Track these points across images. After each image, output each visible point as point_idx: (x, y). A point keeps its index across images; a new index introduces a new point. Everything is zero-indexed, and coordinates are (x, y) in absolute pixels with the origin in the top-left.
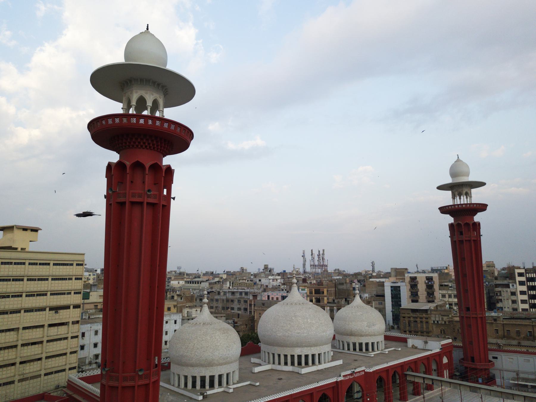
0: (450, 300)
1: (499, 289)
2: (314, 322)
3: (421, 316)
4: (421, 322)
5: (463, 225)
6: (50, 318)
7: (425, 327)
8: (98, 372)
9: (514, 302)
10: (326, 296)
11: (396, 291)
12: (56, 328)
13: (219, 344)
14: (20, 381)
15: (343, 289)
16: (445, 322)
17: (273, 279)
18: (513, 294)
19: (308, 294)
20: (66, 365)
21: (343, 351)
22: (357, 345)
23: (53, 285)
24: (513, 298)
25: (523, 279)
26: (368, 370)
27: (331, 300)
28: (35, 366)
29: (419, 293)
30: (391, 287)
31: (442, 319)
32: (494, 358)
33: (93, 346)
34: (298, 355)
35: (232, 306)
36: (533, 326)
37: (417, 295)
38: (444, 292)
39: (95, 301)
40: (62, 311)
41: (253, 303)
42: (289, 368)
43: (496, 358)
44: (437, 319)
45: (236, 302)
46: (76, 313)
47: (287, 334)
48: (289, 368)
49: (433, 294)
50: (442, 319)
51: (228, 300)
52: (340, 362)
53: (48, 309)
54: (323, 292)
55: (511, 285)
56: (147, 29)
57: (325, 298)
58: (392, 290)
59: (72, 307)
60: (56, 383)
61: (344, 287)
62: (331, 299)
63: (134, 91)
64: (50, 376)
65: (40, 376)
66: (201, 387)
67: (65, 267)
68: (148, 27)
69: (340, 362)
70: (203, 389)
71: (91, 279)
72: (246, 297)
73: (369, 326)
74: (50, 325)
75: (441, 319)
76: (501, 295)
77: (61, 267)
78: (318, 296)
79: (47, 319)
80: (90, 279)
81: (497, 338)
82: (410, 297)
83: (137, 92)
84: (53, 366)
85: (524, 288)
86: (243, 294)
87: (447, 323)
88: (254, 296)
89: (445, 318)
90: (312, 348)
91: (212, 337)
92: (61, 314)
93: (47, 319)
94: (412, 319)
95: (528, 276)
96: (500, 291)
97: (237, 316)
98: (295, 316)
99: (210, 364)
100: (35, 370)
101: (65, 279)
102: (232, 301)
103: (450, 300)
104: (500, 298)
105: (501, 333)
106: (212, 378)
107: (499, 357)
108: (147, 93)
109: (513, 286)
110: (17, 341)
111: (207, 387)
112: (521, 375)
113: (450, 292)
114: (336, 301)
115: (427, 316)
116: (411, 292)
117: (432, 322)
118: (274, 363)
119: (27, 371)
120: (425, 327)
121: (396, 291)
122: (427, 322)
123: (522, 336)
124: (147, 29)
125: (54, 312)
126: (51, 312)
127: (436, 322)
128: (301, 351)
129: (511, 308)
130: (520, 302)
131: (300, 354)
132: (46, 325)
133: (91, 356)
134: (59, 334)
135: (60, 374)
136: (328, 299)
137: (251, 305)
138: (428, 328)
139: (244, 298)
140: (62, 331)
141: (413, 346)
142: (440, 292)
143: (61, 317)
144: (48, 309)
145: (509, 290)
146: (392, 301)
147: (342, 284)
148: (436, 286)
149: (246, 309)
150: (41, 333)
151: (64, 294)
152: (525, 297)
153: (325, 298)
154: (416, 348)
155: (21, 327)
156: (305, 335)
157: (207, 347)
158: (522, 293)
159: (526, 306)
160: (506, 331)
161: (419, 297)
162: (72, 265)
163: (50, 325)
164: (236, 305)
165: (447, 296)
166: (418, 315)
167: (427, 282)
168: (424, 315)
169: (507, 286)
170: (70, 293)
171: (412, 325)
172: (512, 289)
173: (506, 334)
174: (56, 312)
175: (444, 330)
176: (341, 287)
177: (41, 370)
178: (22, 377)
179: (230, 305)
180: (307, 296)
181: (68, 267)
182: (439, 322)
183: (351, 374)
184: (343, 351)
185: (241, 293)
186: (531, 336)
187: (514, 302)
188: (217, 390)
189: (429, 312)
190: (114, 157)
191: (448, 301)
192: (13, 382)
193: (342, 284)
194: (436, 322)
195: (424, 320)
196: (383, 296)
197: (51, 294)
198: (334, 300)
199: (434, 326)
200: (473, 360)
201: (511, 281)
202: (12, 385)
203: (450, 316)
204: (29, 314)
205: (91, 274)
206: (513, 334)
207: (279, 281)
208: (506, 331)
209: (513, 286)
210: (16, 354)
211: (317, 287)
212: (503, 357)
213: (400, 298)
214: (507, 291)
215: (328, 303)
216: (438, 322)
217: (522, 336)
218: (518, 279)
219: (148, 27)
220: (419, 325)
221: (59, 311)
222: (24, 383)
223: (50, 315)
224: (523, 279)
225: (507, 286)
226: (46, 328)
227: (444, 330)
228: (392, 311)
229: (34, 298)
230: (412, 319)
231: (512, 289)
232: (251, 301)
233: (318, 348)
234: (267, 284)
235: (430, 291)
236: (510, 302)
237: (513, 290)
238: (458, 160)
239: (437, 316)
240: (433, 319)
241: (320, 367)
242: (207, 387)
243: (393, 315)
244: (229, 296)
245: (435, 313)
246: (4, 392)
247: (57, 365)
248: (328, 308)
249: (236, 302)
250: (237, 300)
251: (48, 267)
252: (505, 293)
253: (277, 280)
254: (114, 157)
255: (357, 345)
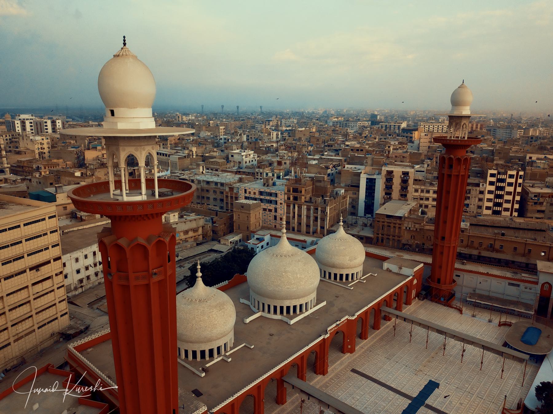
0: (422, 194)
1: (469, 188)
2: (303, 276)
3: (395, 222)
6: (32, 278)
7: (397, 231)
9: (480, 200)
10: (304, 196)
11: (371, 184)
12: (40, 284)
14: (15, 341)
18: (482, 192)
19: (286, 191)
20: (57, 313)
23: (28, 246)
24: (481, 196)
25: (493, 179)
26: (351, 318)
27: (308, 199)
28: (27, 324)
29: (393, 186)
30: (367, 179)
31: (414, 226)
32: (457, 276)
33: (76, 272)
35: (208, 196)
37: (391, 188)
38: (417, 187)
39: (63, 202)
40: (43, 268)
41: (229, 195)
42: (278, 317)
43: (459, 276)
44: (410, 226)
45: (211, 192)
46: (58, 264)
47: (277, 289)
48: (278, 317)
49: (406, 188)
50: (414, 226)
51: (202, 190)
53: (28, 270)
54: (301, 192)
55: (481, 184)
56: (125, 44)
58: (367, 182)
59: (52, 261)
60: (51, 331)
61: (322, 184)
62: (308, 197)
63: (121, 148)
64: (43, 328)
65: (34, 330)
66: (201, 358)
67: (37, 224)
68: (124, 41)
69: (324, 303)
70: (202, 360)
71: (45, 144)
72: (222, 188)
73: (350, 260)
74: (34, 284)
76: (470, 193)
77: (33, 225)
79: (29, 279)
80: (43, 144)
81: (462, 247)
82: (384, 189)
84: (45, 318)
85: (493, 188)
86: (219, 185)
87: (418, 230)
89: (417, 226)
90: (300, 299)
91: (209, 317)
92: (42, 270)
93: (29, 279)
94: (386, 224)
98: (286, 272)
99: (210, 340)
100: (27, 327)
101: (40, 236)
102: (207, 191)
103: (422, 194)
104: (469, 195)
105: (465, 243)
106: (211, 351)
107: (461, 276)
108: (137, 150)
109: (483, 185)
110: (4, 308)
111: (207, 358)
113: (423, 187)
115: (400, 222)
118: (263, 311)
119: (21, 330)
120: (397, 231)
122: (400, 228)
123: (483, 247)
124: (125, 44)
125: (35, 270)
126: (32, 272)
127: (408, 228)
128: (290, 303)
130: (485, 208)
132: (30, 285)
133: (76, 281)
134: (44, 288)
135: (53, 323)
137: (227, 197)
138: (399, 232)
139: (219, 189)
140: (47, 284)
141: (388, 269)
142: (414, 186)
143: (43, 273)
144: (28, 270)
145: (478, 189)
146: (366, 192)
147: (320, 181)
148: (411, 181)
149: (222, 200)
150: (26, 293)
151: (42, 251)
153: (303, 197)
154: (390, 271)
155: (5, 295)
156: (295, 289)
157: (206, 327)
158: (490, 192)
160: (470, 242)
162: (44, 219)
163: (34, 284)
164: (211, 195)
165: (420, 191)
166: (392, 220)
167: (402, 176)
168: (398, 221)
170: (47, 248)
171: (385, 229)
172: (481, 188)
173: (469, 244)
174: (38, 270)
175: (414, 237)
176: (318, 184)
177: (33, 326)
178: (16, 337)
179: (206, 195)
180: (285, 194)
181: (40, 223)
182: (411, 229)
183: (336, 327)
186: (491, 247)
189: (403, 219)
192: (9, 344)
193: (320, 181)
194: (408, 228)
195: (397, 225)
196: (358, 187)
197: (28, 255)
198: (311, 198)
199: (406, 232)
200: (439, 281)
201: (482, 181)
202: (9, 347)
203: (422, 224)
204: (9, 280)
205: (44, 138)
206: (476, 244)
207: (252, 156)
208: (470, 242)
210: (6, 320)
212: (465, 276)
213: (374, 190)
214: (476, 190)
215: (305, 202)
216: (410, 228)
217: (483, 247)
218: (490, 179)
219: (124, 41)
220: (392, 230)
221: (40, 269)
222: (19, 341)
223: (32, 275)
224: (493, 179)
225: (478, 185)
226: (30, 288)
227: (414, 237)
228: (365, 202)
229: (11, 264)
230: (386, 224)
231: (481, 188)
233: (306, 298)
235: (404, 185)
236: (477, 199)
237: (482, 190)
239: (410, 223)
240: (406, 225)
242: (207, 358)
243: (365, 205)
245: (408, 220)
246: (2, 355)
247: (48, 316)
248: (305, 207)
249: (211, 192)
250: (212, 191)
251: (19, 229)
252: (475, 191)
253: (250, 155)
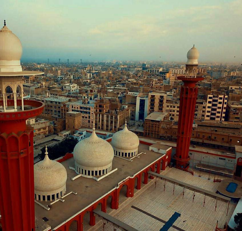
0: (171, 108)
1: (198, 105)
4: (156, 127)
5: (189, 89)
7: (157, 129)
9: (203, 111)
11: (142, 103)
13: (56, 180)
15: (114, 104)
16: (168, 128)
17: (73, 87)
18: (204, 107)
19: (95, 107)
21: (116, 156)
22: (124, 154)
24: (204, 109)
25: (211, 100)
26: (131, 178)
27: (107, 111)
32: (190, 154)
34: (96, 171)
37: (154, 105)
42: (91, 177)
43: (192, 154)
44: (164, 126)
48: (91, 177)
49: (162, 105)
51: (48, 106)
52: (116, 169)
55: (204, 103)
56: (5, 25)
61: (115, 103)
62: (107, 110)
63: (3, 83)
68: (5, 23)
72: (59, 105)
75: (166, 126)
76: (197, 108)
82: (150, 106)
83: (5, 84)
85: (210, 105)
86: (58, 103)
87: (169, 128)
89: (168, 126)
90: (103, 167)
95: (216, 107)
96: (198, 106)
97: (55, 119)
98: (95, 152)
99: (52, 190)
104: (197, 109)
105: (195, 135)
106: (53, 196)
107: (193, 154)
108: (12, 84)
109: (205, 103)
111: (51, 200)
112: (202, 163)
113: (171, 105)
114: (110, 112)
116: (151, 103)
117: (161, 127)
118: (82, 173)
121: (142, 103)
122: (158, 127)
123: (205, 138)
124: (5, 25)
127: (163, 127)
128: (97, 169)
129: (201, 114)
131: (97, 170)
136: (106, 110)
137: (62, 110)
138: (158, 130)
139: (58, 105)
141: (152, 150)
142: (166, 104)
145: (202, 105)
148: (165, 101)
154: (153, 151)
156: (100, 161)
158: (209, 107)
159: (209, 118)
161: (154, 106)
164: (54, 109)
165: (170, 106)
166: (154, 123)
169: (202, 103)
172: (204, 105)
175: (166, 132)
176: (113, 103)
179: (50, 108)
180: (94, 108)
182: (165, 128)
184: (116, 156)
185: (56, 102)
188: (56, 201)
194: (163, 127)
195: (157, 126)
196: (135, 104)
198: (109, 111)
199: (162, 130)
201: (204, 101)
203: (171, 125)
206: (201, 136)
207: (76, 87)
209: (205, 103)
212: (195, 154)
214: (201, 106)
215: (106, 112)
216: (164, 127)
218: (209, 100)
219: (5, 23)
220: (154, 128)
224: (211, 100)
225: (202, 103)
227: (166, 132)
228: (139, 113)
231: (204, 105)
233: (106, 166)
235: (161, 103)
238: (193, 48)
240: (162, 126)
241: (106, 175)
242: (51, 200)
244: (50, 104)
245: (163, 123)
252: (200, 107)
255: (124, 154)
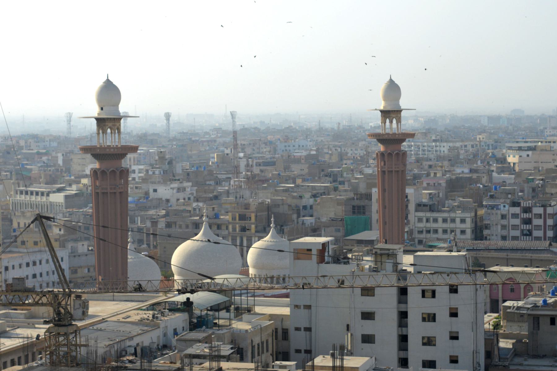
0: (428, 225)
8: (394, 121)
18: (503, 217)
24: (504, 222)
36: (507, 259)
57: (253, 226)
78: (243, 223)
88: (152, 222)
103: (428, 225)
145: (499, 212)
152: (517, 222)
187: (504, 227)
190: (97, 165)
191: (425, 227)
211: (242, 211)
214: (496, 214)
215: (256, 232)
232: (148, 229)
234: (168, 197)
236: (499, 227)
237: (504, 213)
254: (97, 165)
